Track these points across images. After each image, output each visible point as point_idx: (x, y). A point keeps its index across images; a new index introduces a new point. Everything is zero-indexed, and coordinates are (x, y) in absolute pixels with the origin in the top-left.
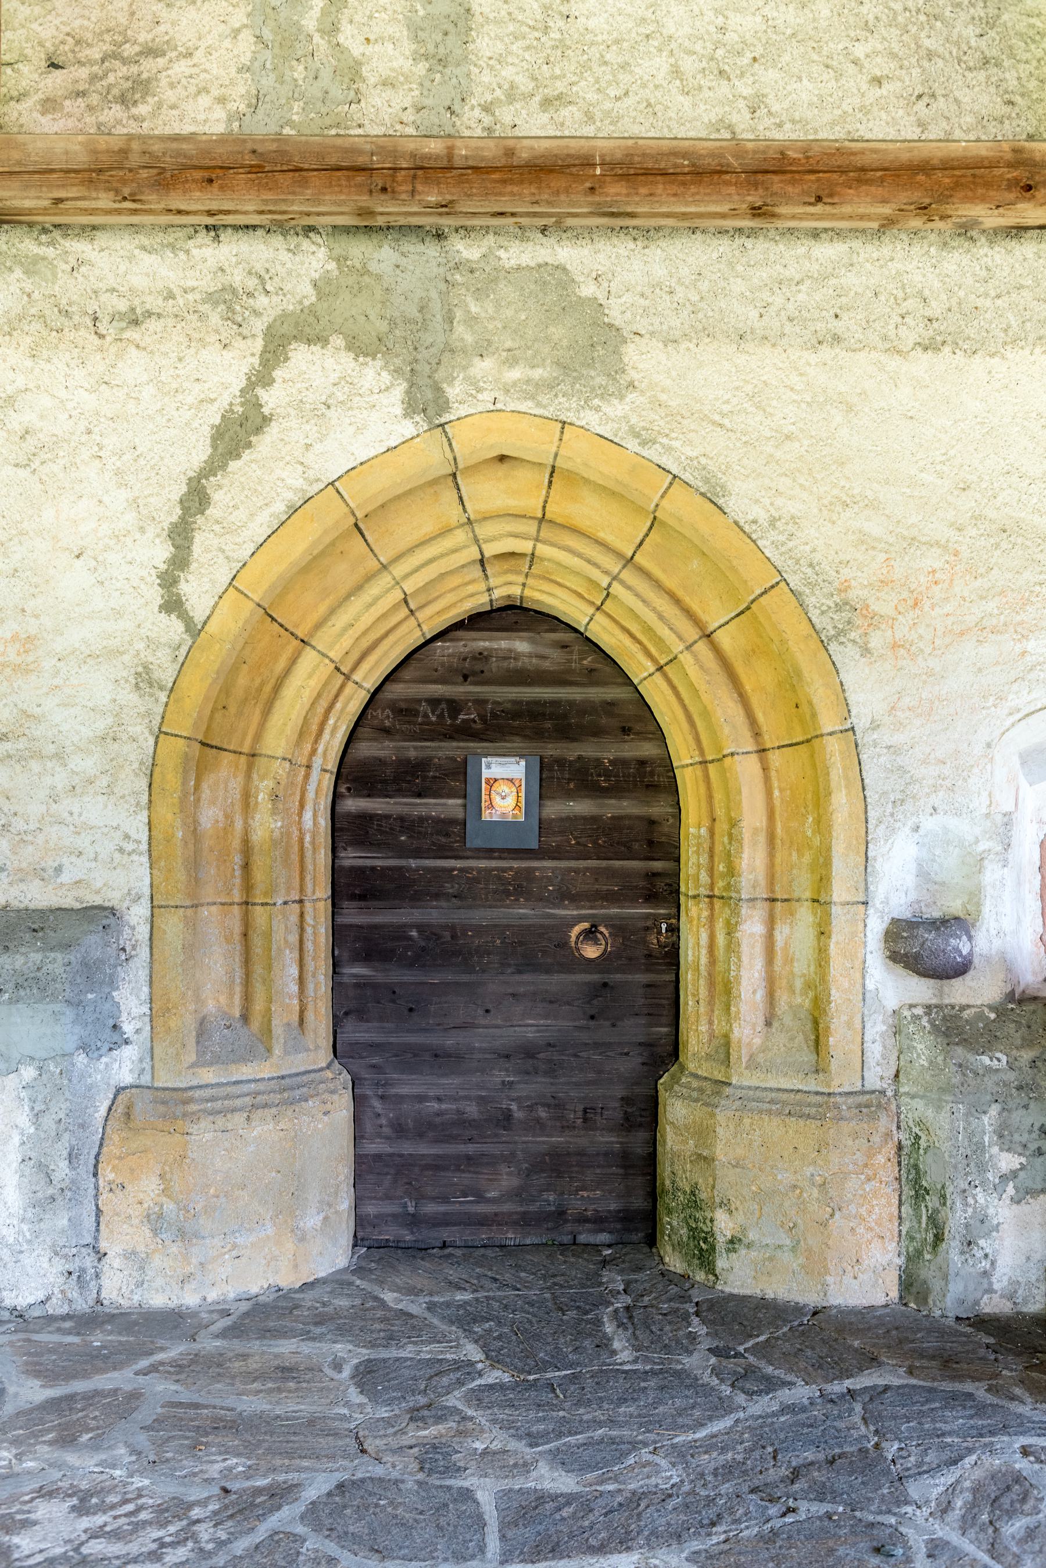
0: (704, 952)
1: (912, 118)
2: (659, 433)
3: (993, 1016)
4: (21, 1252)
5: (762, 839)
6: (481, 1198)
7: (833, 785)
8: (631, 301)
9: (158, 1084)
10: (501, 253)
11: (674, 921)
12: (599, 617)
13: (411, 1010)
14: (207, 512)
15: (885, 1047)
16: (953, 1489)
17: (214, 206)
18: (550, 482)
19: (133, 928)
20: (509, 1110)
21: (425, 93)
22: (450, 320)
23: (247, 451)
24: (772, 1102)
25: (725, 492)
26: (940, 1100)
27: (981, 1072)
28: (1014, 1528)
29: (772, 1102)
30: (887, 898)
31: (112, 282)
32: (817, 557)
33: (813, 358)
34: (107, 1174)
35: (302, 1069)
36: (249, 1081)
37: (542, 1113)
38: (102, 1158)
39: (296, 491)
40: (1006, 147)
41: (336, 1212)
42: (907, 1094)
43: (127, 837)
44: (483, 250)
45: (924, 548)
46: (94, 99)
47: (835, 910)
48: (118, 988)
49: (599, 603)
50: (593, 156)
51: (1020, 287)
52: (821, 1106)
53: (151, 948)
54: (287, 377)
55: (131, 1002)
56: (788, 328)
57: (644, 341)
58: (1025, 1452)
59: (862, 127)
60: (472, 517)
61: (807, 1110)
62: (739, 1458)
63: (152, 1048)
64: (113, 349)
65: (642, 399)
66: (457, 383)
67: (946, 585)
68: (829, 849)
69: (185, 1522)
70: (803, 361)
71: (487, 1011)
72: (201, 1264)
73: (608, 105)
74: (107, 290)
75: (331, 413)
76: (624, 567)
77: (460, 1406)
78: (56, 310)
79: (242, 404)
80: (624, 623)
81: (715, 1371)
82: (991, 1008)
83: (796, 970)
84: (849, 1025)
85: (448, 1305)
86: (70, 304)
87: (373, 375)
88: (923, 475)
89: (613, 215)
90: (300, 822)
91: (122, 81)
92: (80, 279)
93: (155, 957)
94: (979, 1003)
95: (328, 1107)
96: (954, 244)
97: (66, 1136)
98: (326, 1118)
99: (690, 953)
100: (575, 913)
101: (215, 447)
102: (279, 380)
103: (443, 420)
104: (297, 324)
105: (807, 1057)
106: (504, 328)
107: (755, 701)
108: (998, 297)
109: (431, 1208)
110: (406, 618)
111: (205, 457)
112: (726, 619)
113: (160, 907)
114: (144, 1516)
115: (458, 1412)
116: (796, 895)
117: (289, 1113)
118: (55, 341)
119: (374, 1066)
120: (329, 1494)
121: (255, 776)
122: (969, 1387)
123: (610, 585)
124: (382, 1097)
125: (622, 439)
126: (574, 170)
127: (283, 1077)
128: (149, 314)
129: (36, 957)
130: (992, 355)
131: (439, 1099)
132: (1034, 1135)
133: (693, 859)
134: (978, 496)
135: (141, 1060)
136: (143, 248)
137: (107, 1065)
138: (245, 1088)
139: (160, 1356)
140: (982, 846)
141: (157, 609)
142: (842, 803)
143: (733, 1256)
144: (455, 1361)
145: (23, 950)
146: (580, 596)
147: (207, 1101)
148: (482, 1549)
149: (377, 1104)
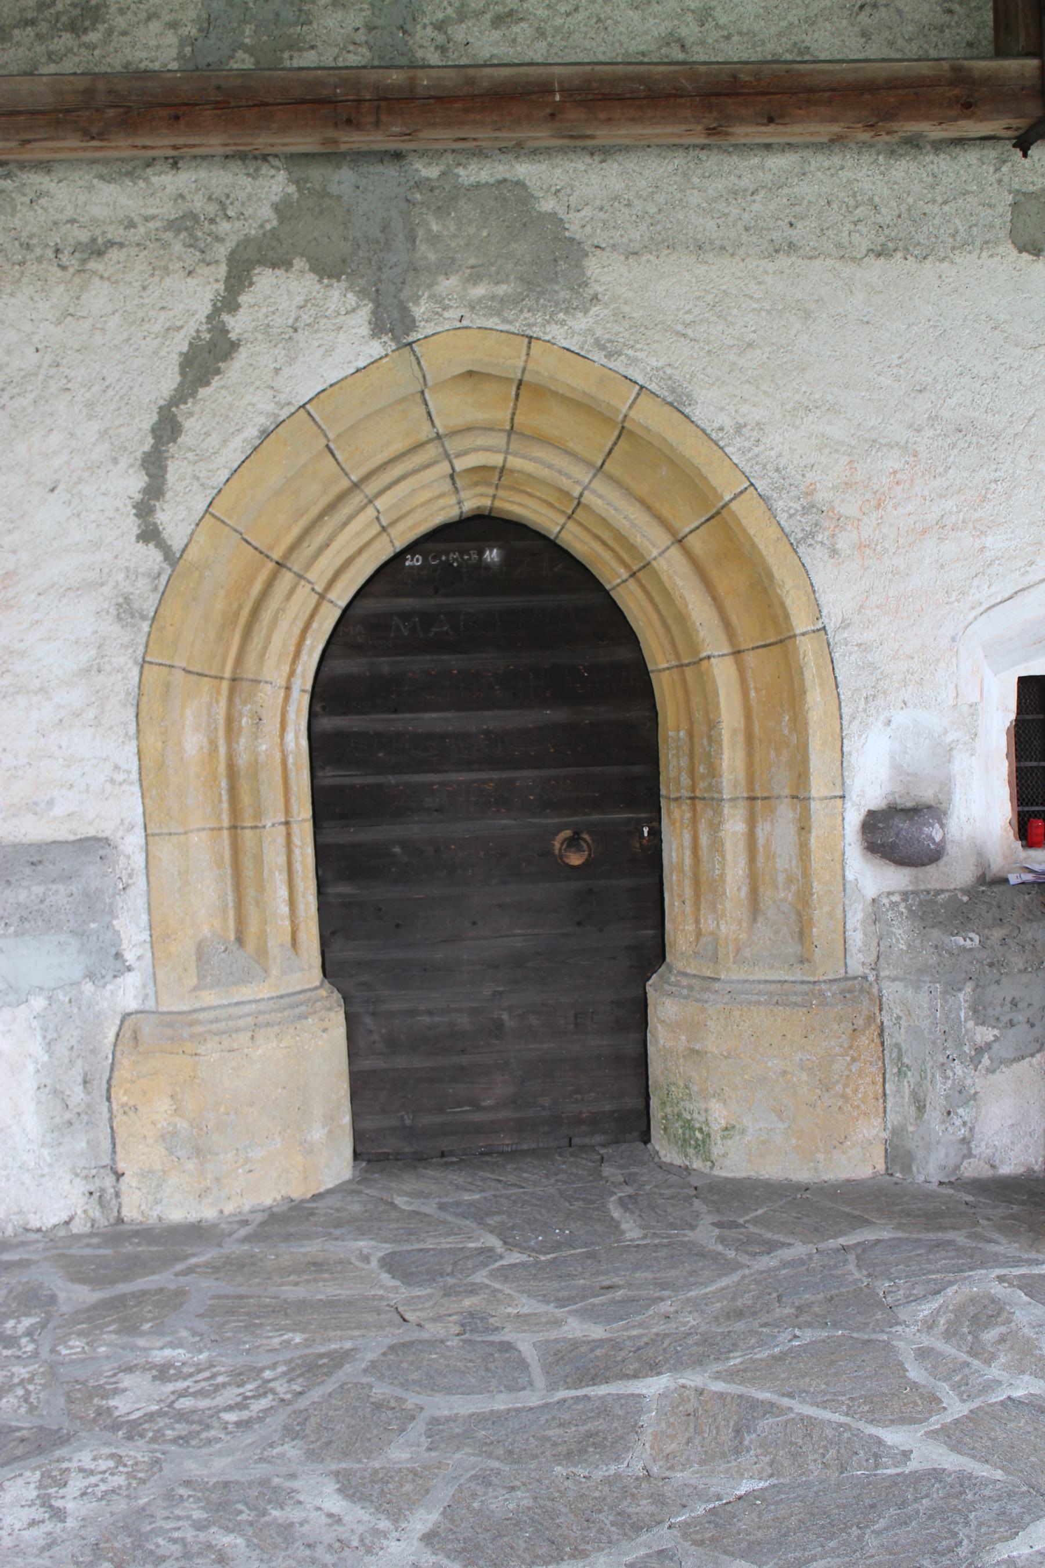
0: (688, 853)
1: (857, 29)
2: (624, 345)
3: (965, 899)
4: (43, 1176)
5: (741, 739)
6: (477, 1108)
7: (808, 683)
8: (590, 214)
9: (164, 1009)
10: (461, 171)
11: (655, 824)
12: (571, 525)
13: (398, 926)
14: (179, 440)
15: (865, 935)
16: (936, 1313)
17: (181, 141)
18: (517, 395)
19: (128, 857)
20: (501, 1020)
21: (377, 13)
22: (412, 238)
23: (217, 378)
24: (760, 993)
25: (692, 402)
26: (919, 980)
27: (956, 952)
28: (990, 1336)
29: (760, 993)
30: (862, 791)
31: (70, 212)
32: (783, 462)
33: (771, 267)
34: (120, 1097)
35: (298, 988)
36: (250, 1002)
37: (533, 1020)
38: (114, 1082)
39: (268, 415)
40: (945, 65)
41: (339, 1126)
42: (888, 977)
43: (117, 767)
44: (442, 168)
45: (885, 449)
46: (44, 27)
47: (814, 805)
48: (117, 917)
49: (570, 512)
50: (552, 83)
51: (966, 193)
52: (806, 994)
53: (148, 876)
54: (252, 301)
55: (132, 931)
56: (744, 238)
57: (606, 254)
58: (1001, 1279)
59: (807, 39)
60: (441, 431)
61: (793, 999)
62: (750, 1302)
63: (154, 974)
64: (77, 280)
65: (606, 311)
66: (422, 301)
67: (907, 486)
68: (806, 747)
69: (259, 1382)
70: (761, 269)
71: (474, 923)
72: (217, 1179)
73: (559, 21)
74: (68, 222)
75: (300, 336)
76: (595, 476)
77: (486, 1281)
78: (16, 243)
79: (209, 331)
80: (595, 531)
81: (721, 1240)
82: (964, 891)
83: (778, 866)
84: (831, 915)
85: (458, 1204)
86: (31, 237)
87: (338, 297)
88: (881, 378)
89: (572, 137)
90: (282, 744)
91: (71, 9)
92: (40, 211)
93: (152, 884)
94: (952, 887)
95: (326, 1023)
96: (901, 152)
97: (79, 1062)
98: (325, 1035)
99: (674, 855)
100: (557, 820)
101: (183, 374)
102: (245, 306)
103: (410, 339)
104: (260, 250)
105: (792, 949)
106: (467, 245)
107: (729, 603)
108: (945, 203)
109: (427, 1120)
110: (378, 535)
111: (175, 386)
112: (696, 524)
113: (154, 835)
114: (220, 1379)
115: (487, 1286)
116: (775, 792)
117: (291, 1030)
118: (18, 275)
119: (364, 984)
120: (384, 1354)
121: (237, 701)
122: (951, 1235)
123: (581, 495)
124: (374, 1014)
125: (588, 351)
126: (534, 97)
127: (282, 997)
128: (111, 244)
129: (39, 890)
130: (942, 260)
131: (430, 1013)
132: (1006, 1008)
133: (673, 762)
134: (933, 397)
135: (144, 986)
136: (101, 177)
137: (112, 992)
138: (247, 1009)
139: (194, 1261)
140: (949, 738)
141: (134, 539)
142: (816, 699)
143: (729, 1142)
144: (476, 1249)
145: (25, 883)
146: (551, 505)
147: (212, 1022)
148: (531, 1383)
149: (368, 1021)
